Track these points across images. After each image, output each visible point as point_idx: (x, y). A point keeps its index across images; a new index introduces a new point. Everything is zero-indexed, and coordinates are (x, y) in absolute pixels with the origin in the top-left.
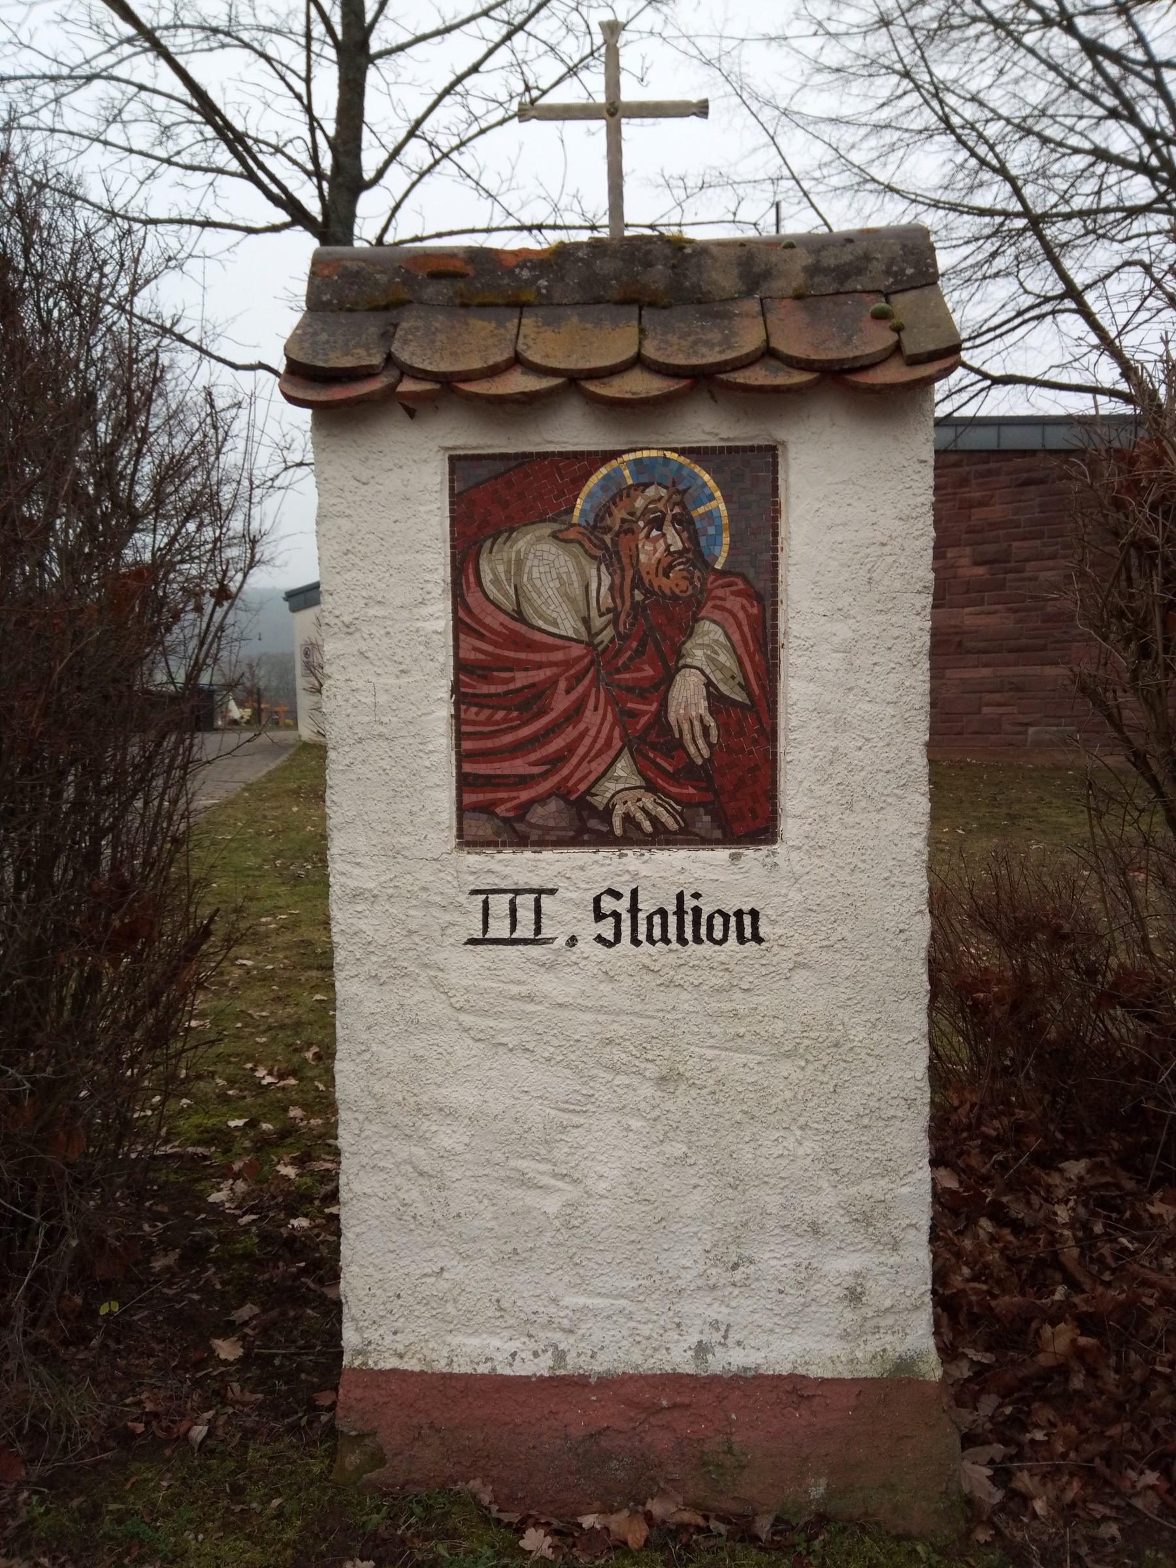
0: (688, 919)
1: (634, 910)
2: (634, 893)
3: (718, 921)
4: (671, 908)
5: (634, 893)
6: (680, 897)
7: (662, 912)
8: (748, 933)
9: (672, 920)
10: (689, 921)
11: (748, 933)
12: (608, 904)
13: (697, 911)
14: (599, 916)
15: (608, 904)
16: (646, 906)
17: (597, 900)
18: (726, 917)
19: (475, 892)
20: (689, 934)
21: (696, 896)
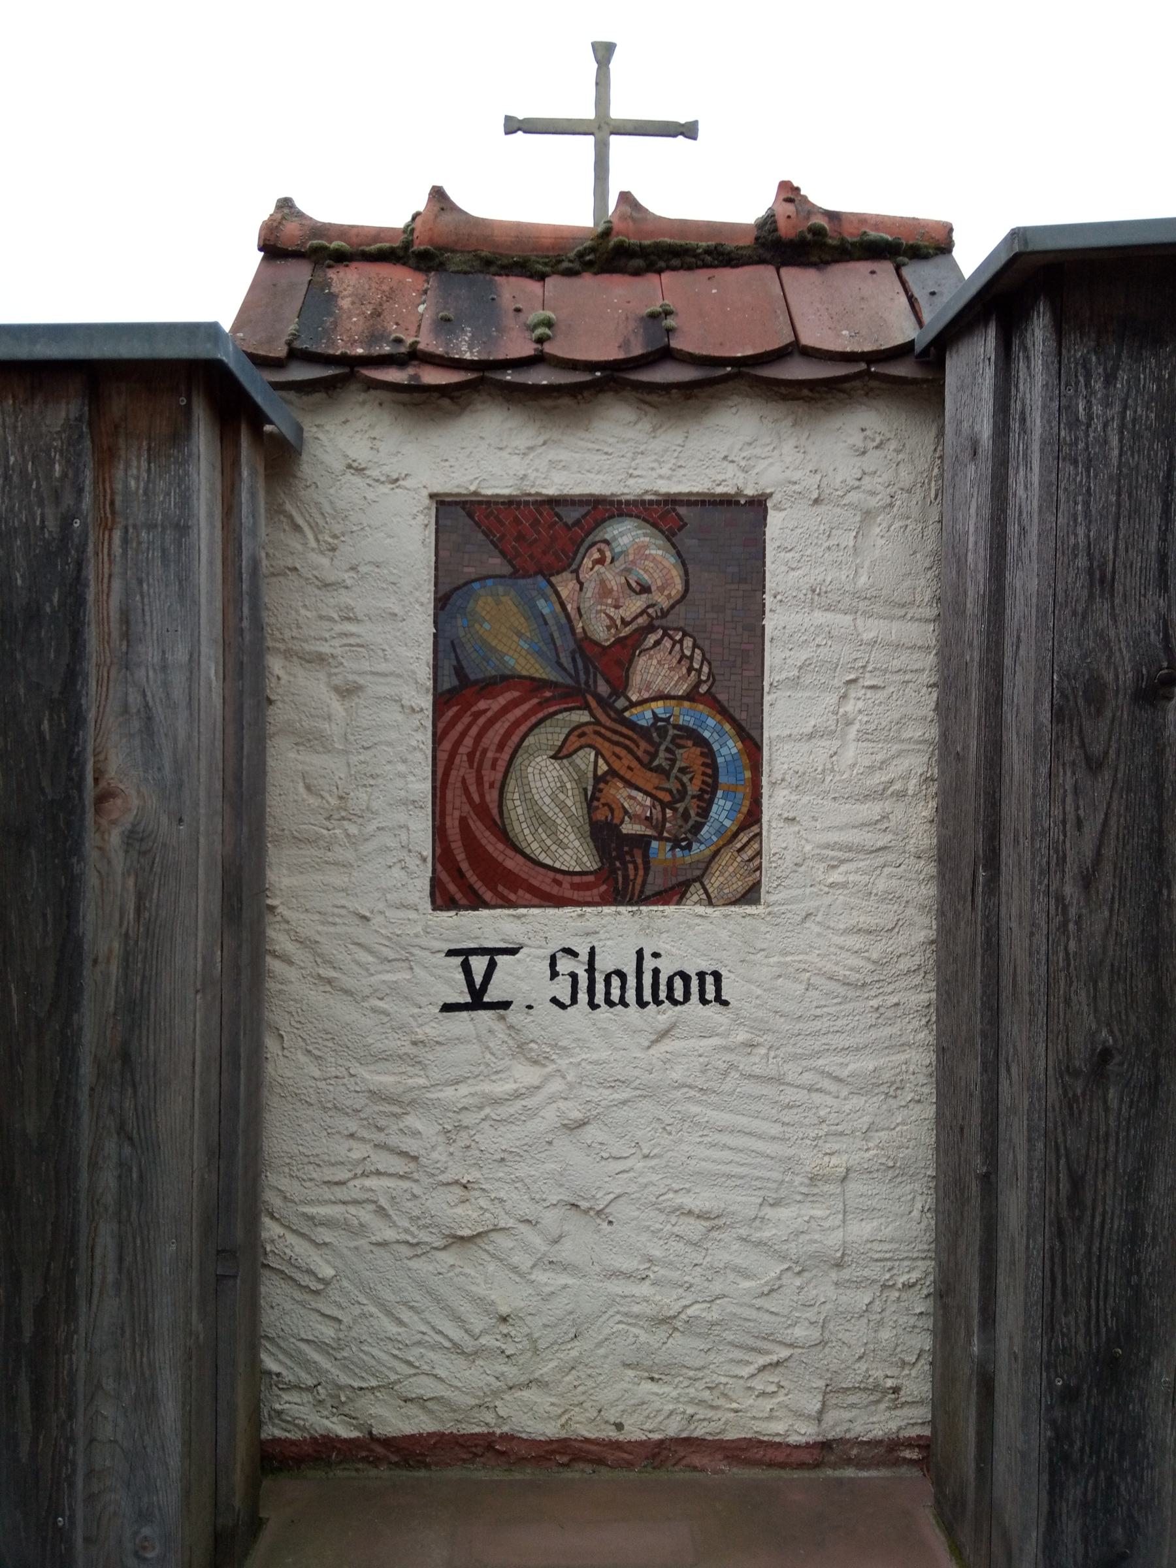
1: (591, 970)
2: (592, 953)
3: (678, 983)
4: (630, 970)
5: (592, 953)
6: (640, 954)
7: (622, 975)
8: (710, 995)
9: (632, 981)
11: (710, 995)
12: (565, 965)
13: (656, 972)
14: (554, 974)
15: (565, 965)
16: (604, 964)
18: (670, 997)
19: (451, 953)
20: (647, 996)
21: (656, 955)
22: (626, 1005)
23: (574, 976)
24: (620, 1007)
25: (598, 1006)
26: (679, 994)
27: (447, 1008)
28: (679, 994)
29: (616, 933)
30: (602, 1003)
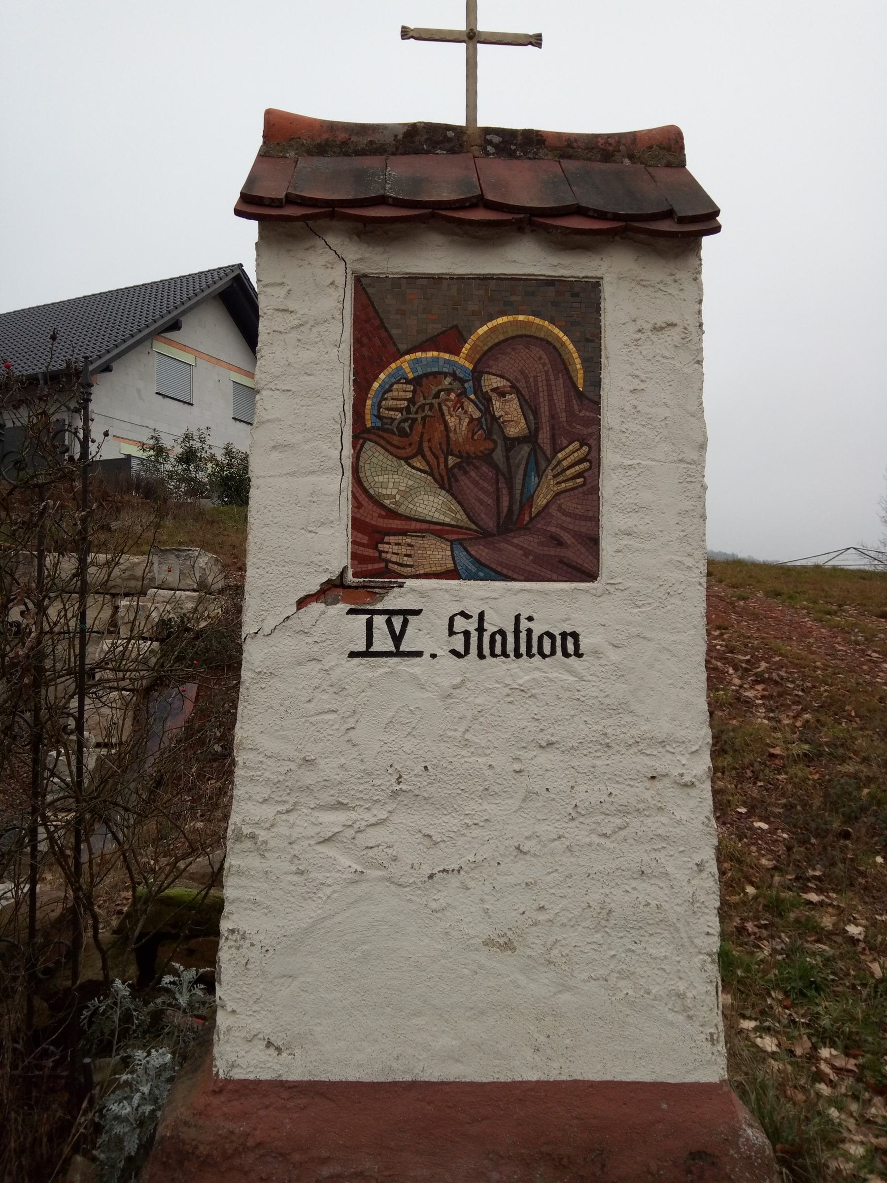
0: (523, 636)
1: (481, 630)
2: (481, 615)
5: (481, 615)
6: (517, 618)
7: (502, 632)
9: (511, 639)
10: (521, 642)
12: (460, 624)
13: (529, 632)
14: (452, 633)
15: (460, 624)
16: (490, 628)
17: (451, 620)
20: (523, 649)
21: (530, 619)
22: (507, 656)
23: (467, 634)
24: (573, 657)
25: (521, 655)
26: (547, 649)
27: (353, 655)
28: (547, 649)
29: (501, 601)
30: (512, 654)
